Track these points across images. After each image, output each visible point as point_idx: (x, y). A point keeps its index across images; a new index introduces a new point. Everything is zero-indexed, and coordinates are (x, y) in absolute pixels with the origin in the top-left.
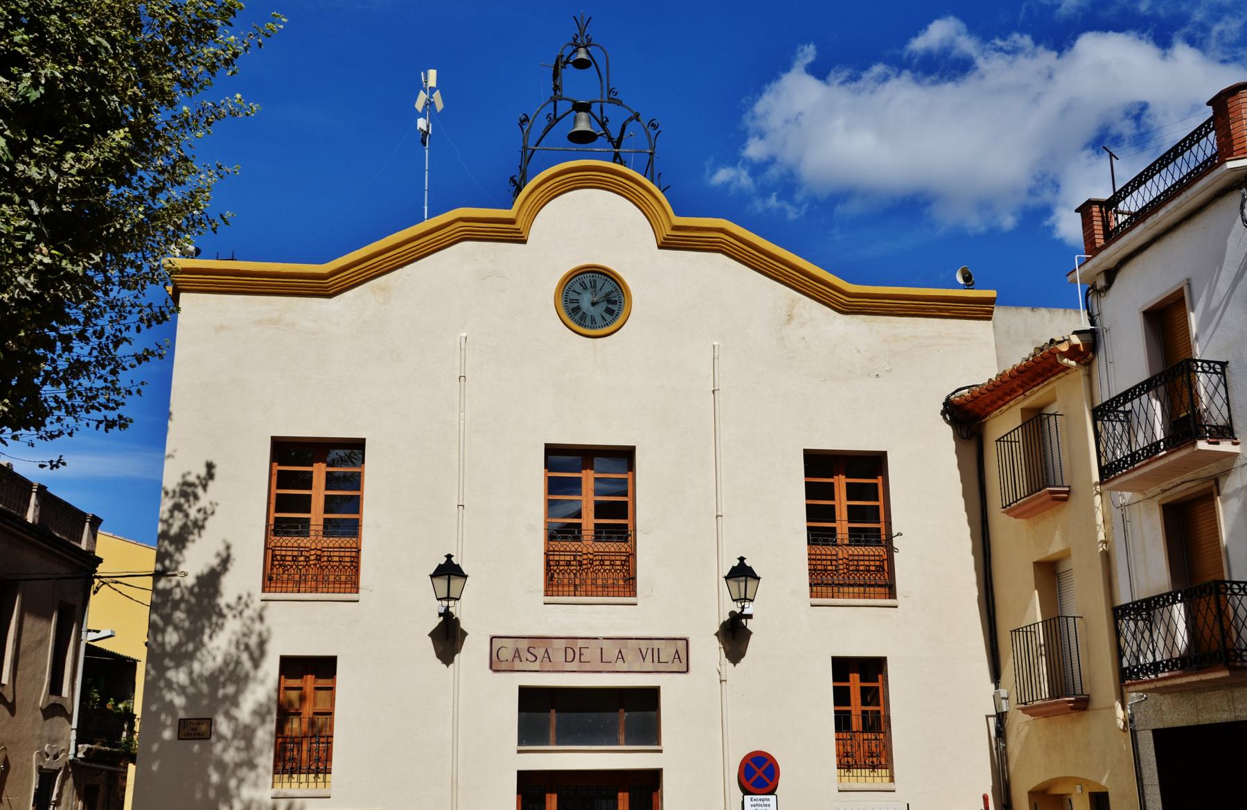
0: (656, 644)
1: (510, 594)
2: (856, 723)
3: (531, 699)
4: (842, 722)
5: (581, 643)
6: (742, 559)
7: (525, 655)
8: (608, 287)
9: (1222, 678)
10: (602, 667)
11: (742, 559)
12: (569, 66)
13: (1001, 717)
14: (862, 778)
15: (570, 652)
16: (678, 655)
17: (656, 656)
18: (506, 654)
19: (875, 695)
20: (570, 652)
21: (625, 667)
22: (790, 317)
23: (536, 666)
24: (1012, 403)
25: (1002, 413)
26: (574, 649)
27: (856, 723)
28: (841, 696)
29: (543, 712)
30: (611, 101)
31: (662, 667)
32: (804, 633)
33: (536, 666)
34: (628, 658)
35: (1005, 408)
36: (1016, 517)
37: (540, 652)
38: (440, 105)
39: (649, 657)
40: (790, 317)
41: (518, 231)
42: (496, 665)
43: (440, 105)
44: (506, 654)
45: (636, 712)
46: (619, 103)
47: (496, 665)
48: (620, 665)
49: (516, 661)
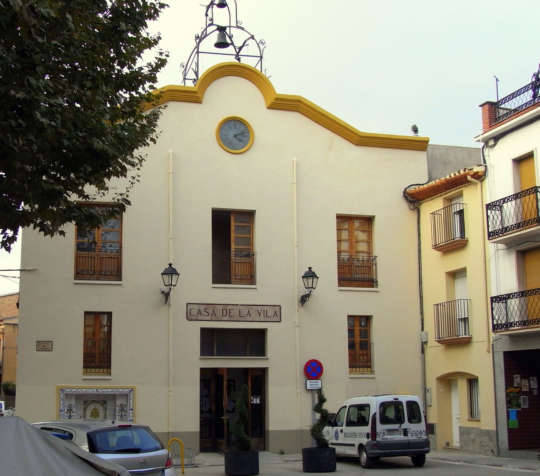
0: (266, 308)
1: (197, 282)
2: (358, 346)
3: (207, 335)
4: (351, 346)
5: (230, 307)
6: (310, 268)
7: (203, 312)
8: (242, 129)
9: (455, 233)
10: (240, 319)
11: (310, 268)
12: (215, 6)
13: (424, 344)
14: (360, 374)
15: (225, 311)
16: (276, 313)
17: (266, 313)
18: (194, 312)
19: (366, 332)
20: (225, 311)
21: (251, 319)
22: (331, 148)
23: (208, 318)
24: (438, 195)
25: (432, 199)
26: (227, 311)
27: (358, 346)
28: (351, 331)
29: (213, 341)
30: (238, 27)
31: (268, 319)
32: (339, 303)
33: (208, 318)
34: (253, 314)
35: (434, 197)
36: (439, 251)
37: (210, 311)
38: (535, 392)
39: (262, 314)
40: (331, 148)
41: (198, 97)
42: (190, 317)
43: (535, 392)
44: (194, 312)
45: (254, 342)
46: (243, 29)
47: (190, 317)
48: (249, 318)
49: (199, 315)
